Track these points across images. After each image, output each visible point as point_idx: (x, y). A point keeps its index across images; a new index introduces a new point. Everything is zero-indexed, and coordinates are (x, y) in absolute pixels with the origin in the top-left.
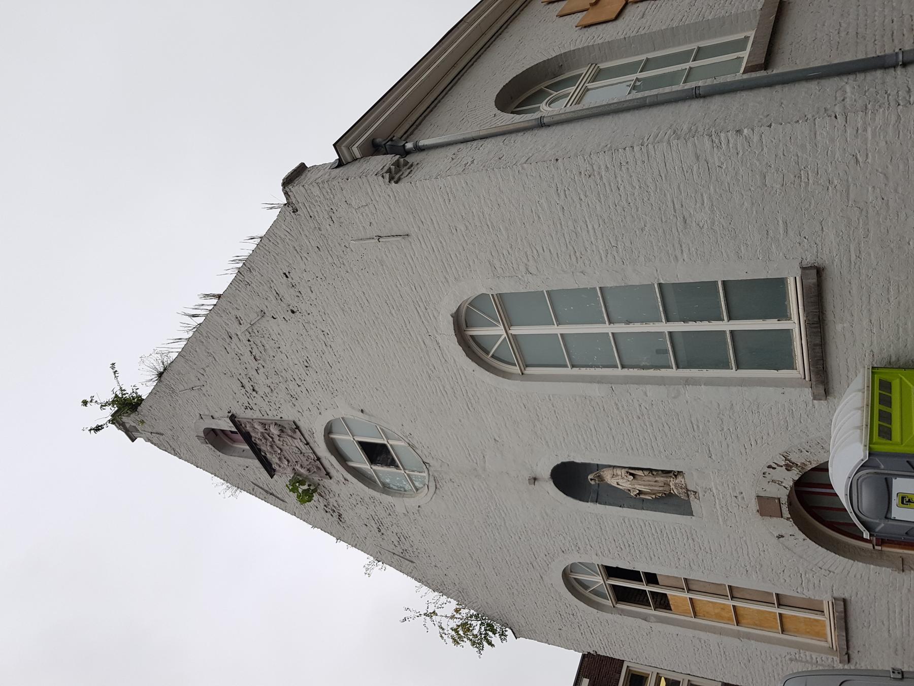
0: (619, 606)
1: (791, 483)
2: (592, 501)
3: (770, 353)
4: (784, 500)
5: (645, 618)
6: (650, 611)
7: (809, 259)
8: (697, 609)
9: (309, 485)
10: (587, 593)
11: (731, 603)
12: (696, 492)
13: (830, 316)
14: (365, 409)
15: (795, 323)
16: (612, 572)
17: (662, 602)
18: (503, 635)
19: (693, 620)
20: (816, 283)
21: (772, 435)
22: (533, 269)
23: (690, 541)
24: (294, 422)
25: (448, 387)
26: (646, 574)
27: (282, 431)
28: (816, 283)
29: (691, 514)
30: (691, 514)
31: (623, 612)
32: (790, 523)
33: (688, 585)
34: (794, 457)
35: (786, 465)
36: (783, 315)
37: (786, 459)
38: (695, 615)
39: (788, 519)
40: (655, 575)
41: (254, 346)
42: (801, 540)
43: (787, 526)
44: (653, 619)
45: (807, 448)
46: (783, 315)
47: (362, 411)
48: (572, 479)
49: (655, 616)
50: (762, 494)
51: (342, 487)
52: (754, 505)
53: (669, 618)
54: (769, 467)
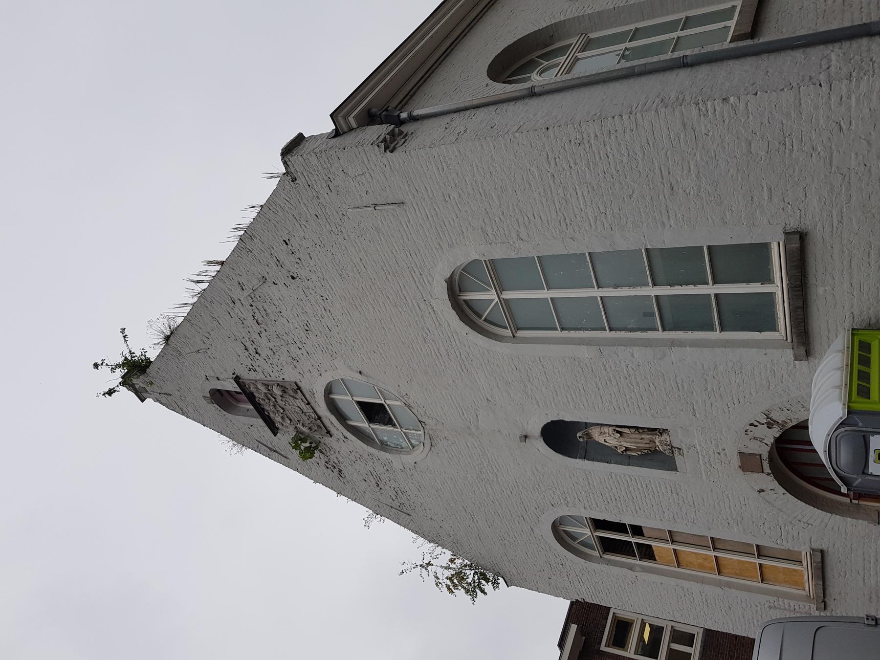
0: (605, 556)
1: (772, 440)
2: (580, 458)
3: (754, 316)
4: (765, 456)
5: (631, 568)
6: (636, 562)
7: (793, 224)
8: (680, 559)
9: (311, 443)
10: (575, 544)
11: (713, 554)
12: (680, 449)
13: (812, 280)
14: (364, 371)
15: (778, 287)
16: (599, 524)
17: (647, 553)
18: (495, 583)
19: (677, 569)
20: (799, 246)
21: (754, 394)
22: (524, 235)
23: (674, 495)
24: (296, 383)
25: (442, 349)
26: (632, 526)
27: (284, 391)
28: (799, 246)
29: (676, 470)
30: (676, 470)
31: (609, 562)
32: (771, 478)
33: (672, 536)
34: (776, 416)
35: (768, 423)
36: (767, 279)
37: (768, 418)
38: (719, 573)
39: (769, 474)
40: (640, 527)
41: (256, 311)
42: (781, 494)
43: (768, 481)
44: (638, 568)
45: (788, 406)
46: (767, 279)
47: (360, 373)
48: (561, 436)
49: (640, 566)
50: (744, 451)
51: (342, 445)
52: (736, 461)
53: (656, 568)
54: (751, 425)
